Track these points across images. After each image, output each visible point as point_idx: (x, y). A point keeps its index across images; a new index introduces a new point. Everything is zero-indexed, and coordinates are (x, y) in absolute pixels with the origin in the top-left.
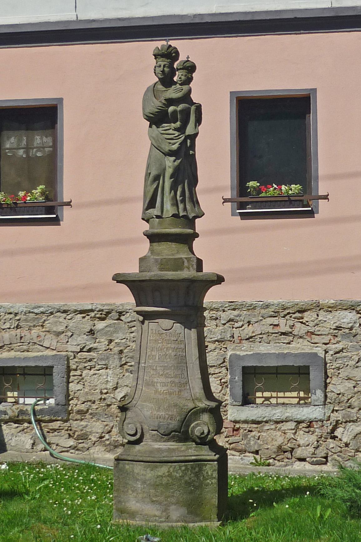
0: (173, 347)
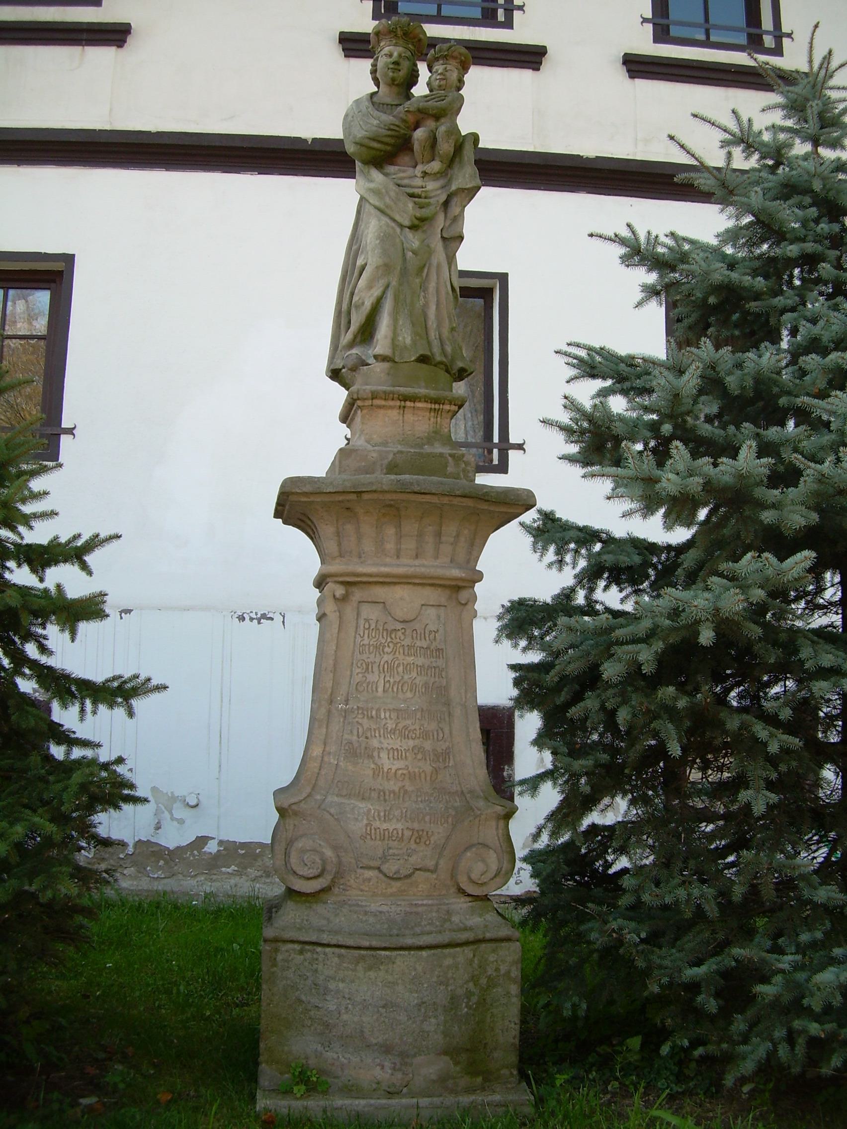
0: (420, 663)
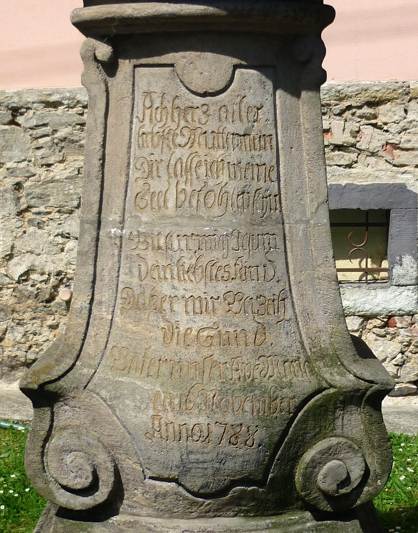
0: (233, 159)
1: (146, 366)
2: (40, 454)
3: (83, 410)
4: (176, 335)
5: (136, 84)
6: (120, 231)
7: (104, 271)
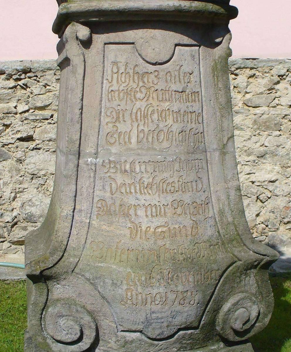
0: (175, 109)
1: (119, 254)
2: (39, 320)
3: (71, 287)
4: (139, 232)
5: (105, 56)
6: (95, 160)
7: (83, 189)
